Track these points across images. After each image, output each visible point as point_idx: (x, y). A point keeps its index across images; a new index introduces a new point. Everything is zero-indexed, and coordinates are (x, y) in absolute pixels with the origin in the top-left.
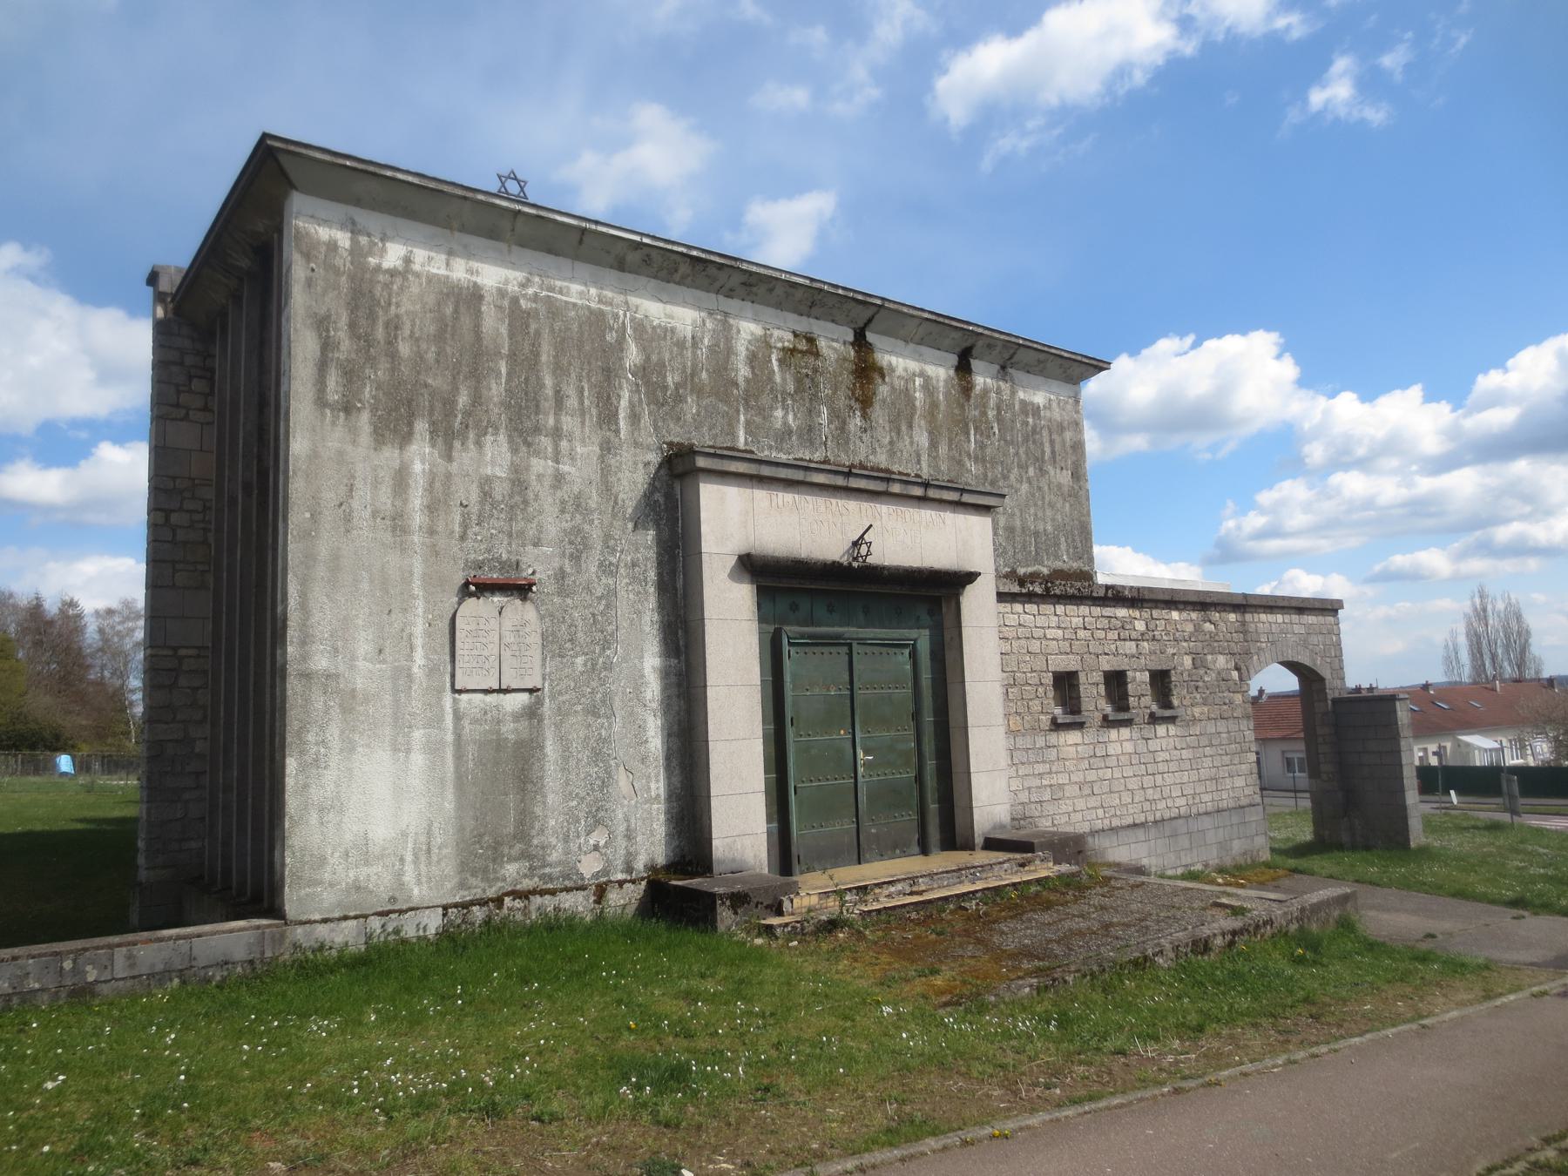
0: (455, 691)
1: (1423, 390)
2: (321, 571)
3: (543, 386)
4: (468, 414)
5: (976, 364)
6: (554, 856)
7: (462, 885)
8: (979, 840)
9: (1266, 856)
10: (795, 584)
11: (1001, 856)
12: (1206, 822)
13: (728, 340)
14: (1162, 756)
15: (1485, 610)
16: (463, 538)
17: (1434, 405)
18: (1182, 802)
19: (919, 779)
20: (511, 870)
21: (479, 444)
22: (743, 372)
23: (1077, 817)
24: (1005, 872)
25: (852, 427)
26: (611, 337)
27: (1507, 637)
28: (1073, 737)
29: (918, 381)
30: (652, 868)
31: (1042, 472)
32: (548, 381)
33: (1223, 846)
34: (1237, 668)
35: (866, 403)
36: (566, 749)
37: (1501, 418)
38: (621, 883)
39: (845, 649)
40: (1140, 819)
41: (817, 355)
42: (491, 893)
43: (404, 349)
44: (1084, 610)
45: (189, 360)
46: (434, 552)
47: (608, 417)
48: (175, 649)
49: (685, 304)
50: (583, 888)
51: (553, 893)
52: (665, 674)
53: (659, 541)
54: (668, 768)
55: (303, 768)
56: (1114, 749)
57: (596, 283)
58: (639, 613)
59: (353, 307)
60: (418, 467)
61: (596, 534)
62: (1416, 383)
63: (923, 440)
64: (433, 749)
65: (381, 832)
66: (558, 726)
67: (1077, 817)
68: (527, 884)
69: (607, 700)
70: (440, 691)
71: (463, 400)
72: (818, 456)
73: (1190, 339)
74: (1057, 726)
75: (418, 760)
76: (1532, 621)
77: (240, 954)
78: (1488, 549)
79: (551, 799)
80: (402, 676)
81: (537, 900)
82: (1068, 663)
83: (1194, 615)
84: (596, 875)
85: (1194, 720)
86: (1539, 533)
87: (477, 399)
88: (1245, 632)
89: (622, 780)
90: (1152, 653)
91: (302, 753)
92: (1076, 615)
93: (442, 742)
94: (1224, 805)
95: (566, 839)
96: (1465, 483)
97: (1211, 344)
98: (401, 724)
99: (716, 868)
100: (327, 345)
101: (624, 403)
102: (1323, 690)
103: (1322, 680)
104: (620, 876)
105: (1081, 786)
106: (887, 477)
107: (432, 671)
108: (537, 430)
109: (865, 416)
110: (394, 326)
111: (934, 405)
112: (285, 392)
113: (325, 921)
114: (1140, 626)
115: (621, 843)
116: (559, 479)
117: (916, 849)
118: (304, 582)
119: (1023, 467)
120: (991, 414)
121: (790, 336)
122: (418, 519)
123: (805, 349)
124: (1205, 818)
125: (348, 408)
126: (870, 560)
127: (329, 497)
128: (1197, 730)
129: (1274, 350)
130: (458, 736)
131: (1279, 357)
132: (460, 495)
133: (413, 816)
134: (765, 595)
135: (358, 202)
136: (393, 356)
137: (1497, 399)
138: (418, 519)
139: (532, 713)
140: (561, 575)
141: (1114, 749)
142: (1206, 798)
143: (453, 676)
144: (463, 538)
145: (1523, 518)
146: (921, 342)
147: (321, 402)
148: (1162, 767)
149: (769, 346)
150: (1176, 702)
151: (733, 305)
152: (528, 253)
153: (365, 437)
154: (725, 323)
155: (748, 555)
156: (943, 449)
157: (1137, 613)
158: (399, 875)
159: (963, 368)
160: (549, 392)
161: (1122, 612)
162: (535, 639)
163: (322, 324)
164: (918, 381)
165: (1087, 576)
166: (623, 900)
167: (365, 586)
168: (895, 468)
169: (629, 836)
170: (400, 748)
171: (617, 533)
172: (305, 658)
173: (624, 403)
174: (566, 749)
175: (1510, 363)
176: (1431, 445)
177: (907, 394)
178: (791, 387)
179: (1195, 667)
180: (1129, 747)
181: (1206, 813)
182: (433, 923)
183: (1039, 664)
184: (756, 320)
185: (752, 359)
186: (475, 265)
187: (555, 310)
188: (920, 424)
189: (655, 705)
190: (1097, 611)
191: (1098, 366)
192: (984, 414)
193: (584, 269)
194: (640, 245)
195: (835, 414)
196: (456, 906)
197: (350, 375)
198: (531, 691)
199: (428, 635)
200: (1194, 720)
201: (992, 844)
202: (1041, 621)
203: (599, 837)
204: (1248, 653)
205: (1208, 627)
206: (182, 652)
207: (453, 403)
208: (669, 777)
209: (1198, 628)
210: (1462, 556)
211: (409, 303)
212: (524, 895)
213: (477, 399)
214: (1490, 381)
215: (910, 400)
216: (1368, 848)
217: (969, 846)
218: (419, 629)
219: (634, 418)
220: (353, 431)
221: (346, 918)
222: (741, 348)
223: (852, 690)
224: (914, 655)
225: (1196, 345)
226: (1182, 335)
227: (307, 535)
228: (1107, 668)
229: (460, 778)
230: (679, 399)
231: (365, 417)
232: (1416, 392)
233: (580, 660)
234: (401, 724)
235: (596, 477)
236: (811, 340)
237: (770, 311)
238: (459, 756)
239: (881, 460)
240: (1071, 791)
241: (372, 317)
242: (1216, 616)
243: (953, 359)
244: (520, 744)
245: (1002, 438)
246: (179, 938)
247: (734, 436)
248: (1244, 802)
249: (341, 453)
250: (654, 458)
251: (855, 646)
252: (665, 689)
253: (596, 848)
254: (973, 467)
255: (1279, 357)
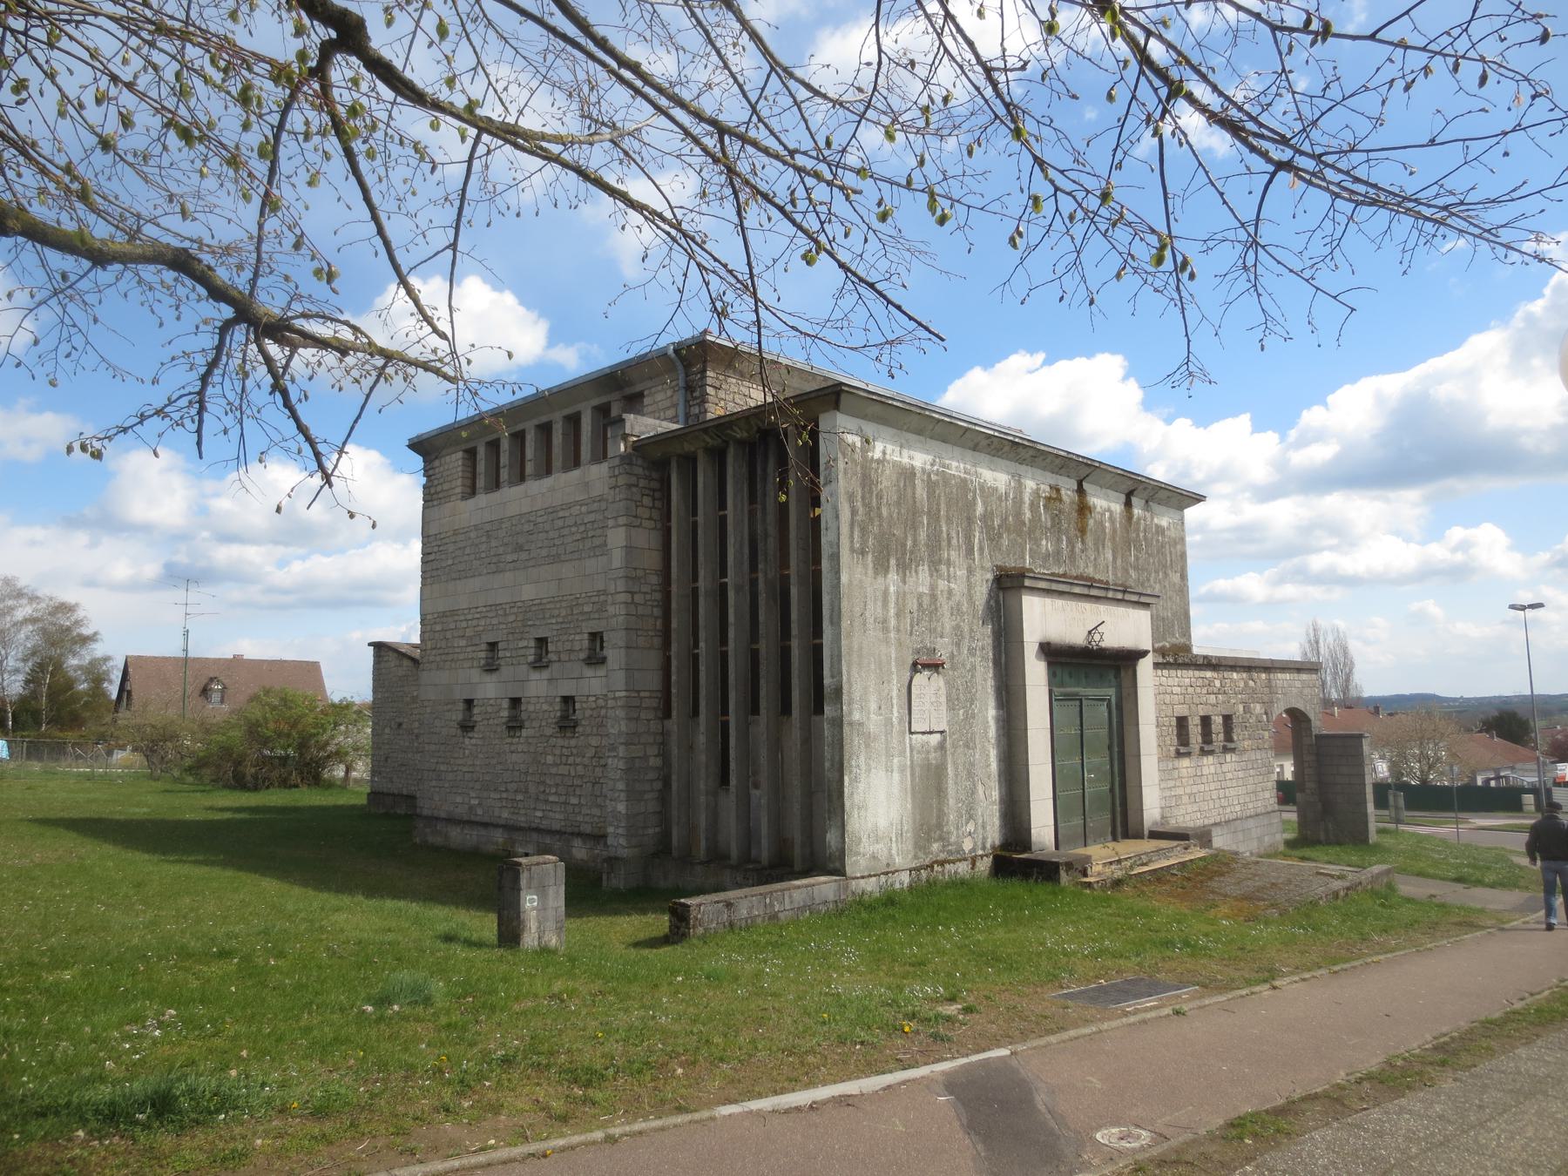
0: (911, 733)
1: (1251, 419)
2: (855, 658)
3: (941, 532)
4: (912, 552)
5: (1134, 500)
6: (953, 839)
7: (916, 857)
8: (1146, 833)
9: (1281, 848)
10: (1081, 661)
11: (1175, 843)
12: (1251, 823)
13: (1021, 493)
14: (1229, 776)
15: (1317, 642)
16: (911, 634)
17: (1262, 435)
18: (1238, 808)
19: (1112, 790)
20: (935, 846)
21: (916, 572)
22: (1028, 515)
23: (1188, 817)
24: (1176, 856)
25: (1077, 550)
26: (970, 496)
27: (1335, 666)
28: (1185, 762)
29: (1107, 514)
30: (993, 847)
31: (1166, 574)
32: (944, 529)
33: (1260, 839)
34: (1266, 713)
35: (1083, 531)
36: (957, 769)
37: (1320, 454)
38: (982, 856)
39: (1078, 703)
40: (1218, 820)
41: (1061, 500)
42: (927, 862)
43: (885, 512)
44: (1191, 673)
45: (642, 483)
46: (900, 644)
47: (970, 551)
48: (638, 692)
49: (1002, 471)
50: (965, 859)
51: (953, 862)
52: (998, 720)
53: (994, 632)
54: (1000, 781)
55: (850, 779)
56: (1206, 771)
57: (963, 460)
58: (985, 680)
59: (863, 486)
60: (892, 589)
61: (966, 629)
62: (1245, 412)
63: (1109, 556)
64: (902, 770)
65: (883, 823)
66: (953, 754)
67: (1188, 818)
68: (942, 856)
69: (973, 739)
70: (904, 733)
71: (909, 543)
72: (1061, 571)
73: (1041, 357)
74: (1179, 755)
75: (896, 776)
76: (1354, 647)
77: (831, 897)
78: (1304, 576)
79: (951, 802)
80: (888, 722)
81: (947, 866)
82: (1182, 710)
83: (1244, 675)
84: (970, 852)
85: (1245, 750)
86: (1350, 564)
87: (915, 541)
88: (1270, 687)
89: (980, 789)
90: (1224, 702)
91: (851, 772)
92: (1188, 676)
93: (905, 765)
94: (1259, 811)
95: (958, 829)
96: (1284, 514)
97: (1062, 365)
98: (889, 756)
99: (1034, 848)
100: (854, 512)
101: (977, 541)
102: (1310, 729)
103: (1310, 721)
104: (980, 852)
105: (1190, 795)
106: (1091, 583)
107: (901, 720)
108: (940, 561)
109: (1083, 542)
110: (880, 497)
111: (1114, 530)
112: (831, 544)
113: (863, 877)
114: (1217, 683)
115: (980, 830)
116: (950, 592)
117: (1110, 838)
118: (849, 666)
119: (1157, 572)
120: (1142, 535)
121: (1048, 489)
122: (893, 622)
123: (1054, 498)
124: (1251, 820)
125: (863, 553)
126: (1103, 645)
127: (857, 610)
128: (1245, 757)
129: (1120, 373)
130: (912, 761)
131: (1125, 378)
132: (909, 607)
133: (895, 814)
134: (1050, 665)
135: (864, 417)
136: (880, 516)
137: (1320, 436)
138: (893, 622)
139: (941, 746)
140: (952, 656)
141: (1206, 771)
142: (1251, 805)
143: (910, 723)
144: (911, 634)
145: (1331, 548)
146: (1109, 488)
147: (852, 550)
148: (1229, 784)
149: (1039, 497)
150: (1235, 738)
151: (1023, 469)
152: (934, 442)
153: (870, 572)
154: (1019, 481)
155: (1048, 644)
156: (1119, 562)
157: (1215, 675)
158: (890, 849)
159: (1128, 504)
160: (945, 535)
161: (1209, 674)
162: (943, 699)
163: (851, 497)
164: (1107, 514)
165: (1187, 648)
166: (984, 865)
167: (873, 667)
168: (1097, 577)
169: (984, 827)
170: (889, 770)
171: (975, 628)
172: (850, 713)
173: (977, 541)
174: (957, 769)
175: (1330, 399)
176: (1260, 473)
177: (1101, 524)
178: (1049, 524)
179: (1245, 712)
180: (1212, 770)
181: (1251, 817)
182: (905, 878)
183: (1169, 713)
184: (1033, 479)
185: (1032, 504)
186: (912, 453)
187: (946, 478)
188: (1108, 544)
189: (993, 741)
190: (1197, 673)
191: (1197, 499)
192: (1138, 535)
193: (957, 450)
194: (990, 436)
195: (1070, 541)
196: (914, 869)
197: (864, 531)
198: (942, 732)
199: (899, 696)
200: (1245, 750)
201: (1154, 835)
202: (1170, 681)
203: (971, 827)
204: (1272, 702)
205: (1251, 683)
206: (642, 694)
207: (905, 545)
208: (1000, 789)
209: (1246, 684)
210: (1281, 581)
211: (886, 481)
212: (942, 863)
213: (915, 541)
214: (1313, 417)
215: (1104, 528)
216: (1339, 843)
217: (1138, 835)
218: (895, 693)
219: (981, 549)
220: (865, 566)
221: (870, 876)
222: (1027, 499)
223: (1082, 730)
224: (1109, 706)
225: (1048, 362)
226: (1032, 351)
227: (849, 636)
228: (1202, 714)
229: (913, 789)
230: (1000, 536)
231: (870, 557)
232: (1244, 420)
233: (961, 712)
234: (889, 756)
235: (965, 591)
236: (1058, 490)
237: (1039, 472)
238: (912, 775)
239: (1090, 571)
240: (1185, 799)
241: (871, 492)
242: (1255, 675)
243: (1123, 497)
244: (937, 767)
245: (1147, 553)
246: (807, 886)
247: (1023, 558)
248: (1270, 809)
249: (861, 581)
250: (990, 576)
251: (1084, 702)
252: (997, 730)
253: (970, 834)
254: (1133, 573)
255: (1125, 378)
